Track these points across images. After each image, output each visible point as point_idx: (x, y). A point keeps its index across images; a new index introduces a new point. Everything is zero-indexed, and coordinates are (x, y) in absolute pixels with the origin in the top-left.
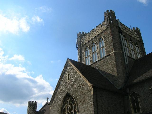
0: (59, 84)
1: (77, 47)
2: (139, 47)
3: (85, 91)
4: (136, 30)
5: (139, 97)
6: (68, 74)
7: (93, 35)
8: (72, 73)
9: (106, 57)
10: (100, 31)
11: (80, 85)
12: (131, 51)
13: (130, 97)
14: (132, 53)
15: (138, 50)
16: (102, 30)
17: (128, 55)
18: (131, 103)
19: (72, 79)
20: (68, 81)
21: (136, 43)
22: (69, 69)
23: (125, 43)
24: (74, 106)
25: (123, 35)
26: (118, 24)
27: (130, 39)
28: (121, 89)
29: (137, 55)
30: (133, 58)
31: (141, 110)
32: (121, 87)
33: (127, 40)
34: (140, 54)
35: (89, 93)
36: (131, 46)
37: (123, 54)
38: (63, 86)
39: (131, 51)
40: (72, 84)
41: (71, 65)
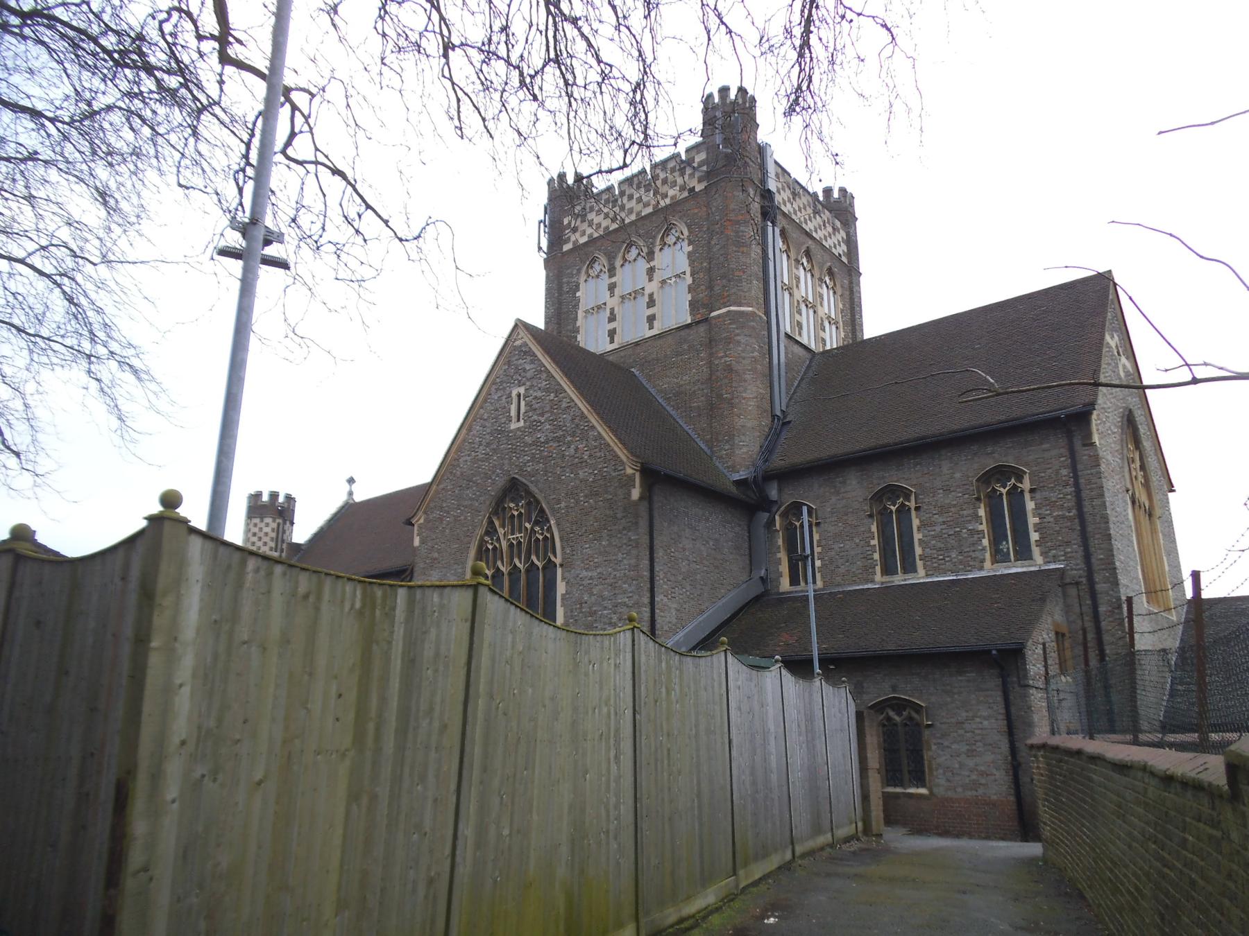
0: (464, 431)
1: (540, 248)
2: (839, 291)
3: (601, 482)
4: (837, 202)
5: (818, 524)
6: (519, 396)
7: (633, 203)
8: (539, 394)
9: (688, 326)
10: (671, 193)
11: (577, 449)
12: (826, 324)
13: (777, 517)
14: (806, 318)
15: (830, 305)
16: (682, 189)
17: (788, 330)
18: (780, 542)
19: (535, 417)
20: (513, 426)
21: (830, 272)
22: (525, 370)
23: (783, 267)
24: (546, 538)
25: (777, 231)
26: (763, 167)
27: (807, 250)
28: (740, 483)
29: (824, 330)
30: (805, 342)
31: (919, 564)
32: (741, 475)
33: (792, 255)
34: (836, 323)
35: (620, 492)
36: (806, 287)
37: (769, 322)
38: (488, 445)
39: (826, 324)
40: (536, 443)
41: (534, 355)
